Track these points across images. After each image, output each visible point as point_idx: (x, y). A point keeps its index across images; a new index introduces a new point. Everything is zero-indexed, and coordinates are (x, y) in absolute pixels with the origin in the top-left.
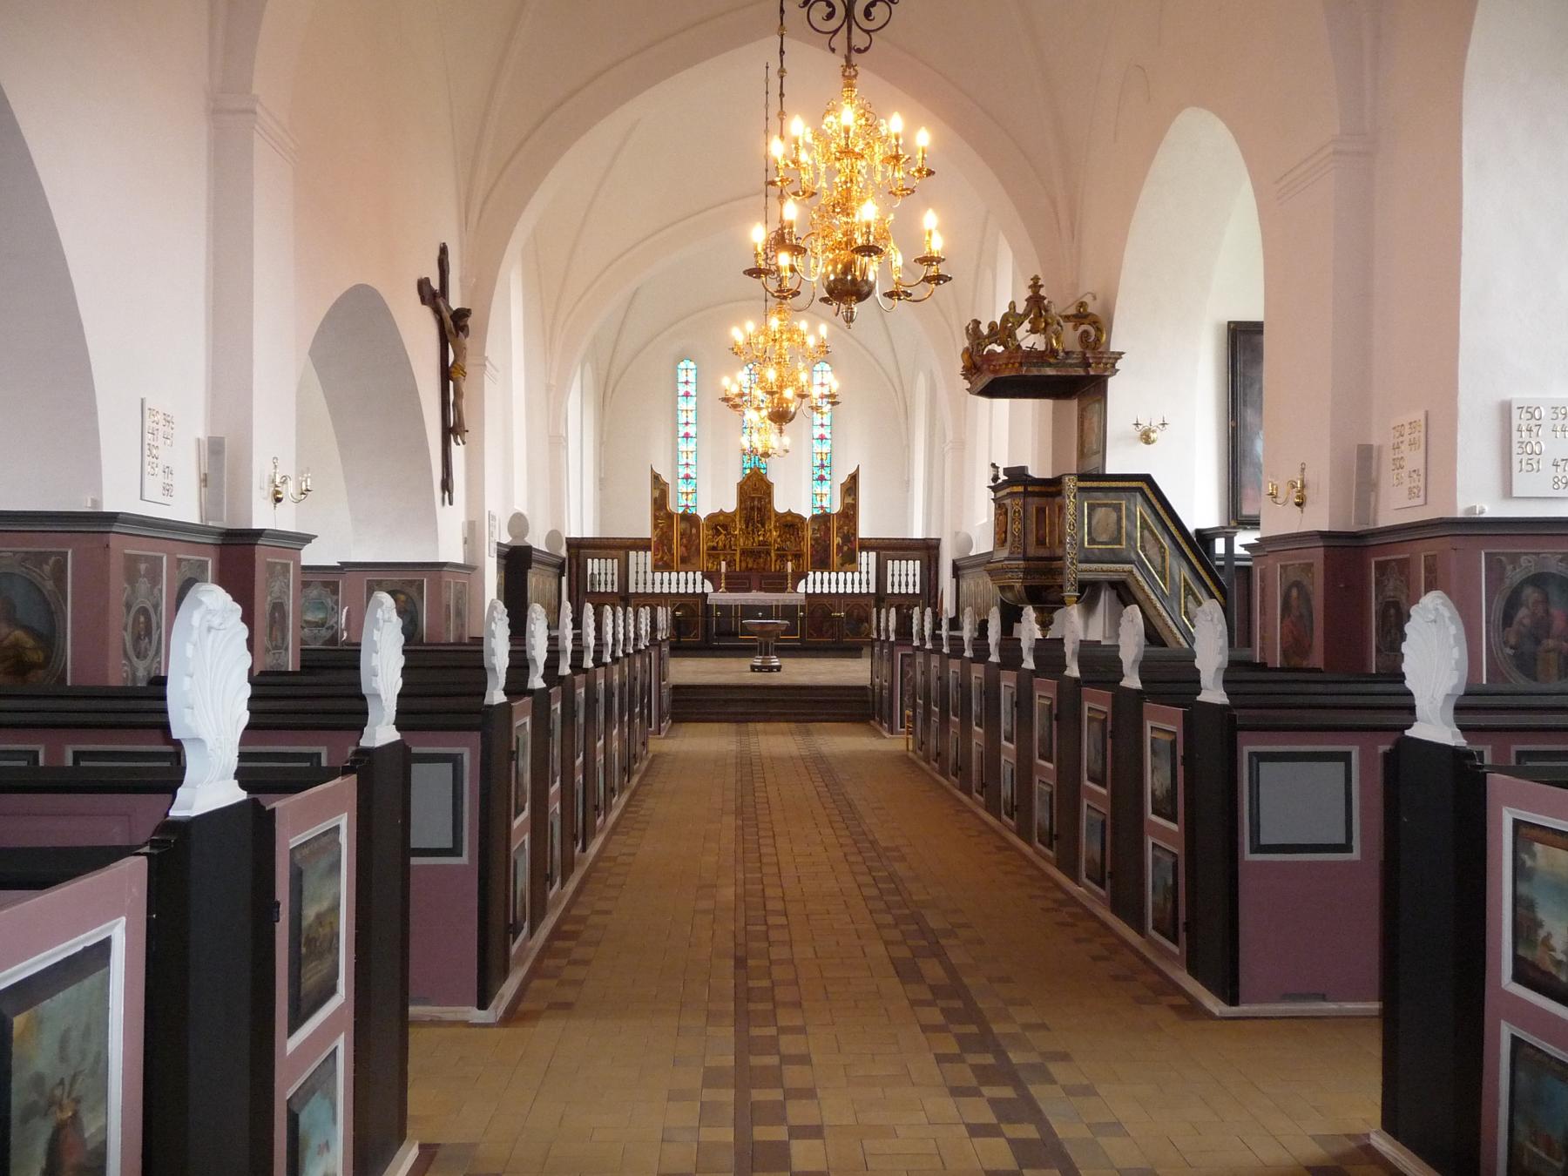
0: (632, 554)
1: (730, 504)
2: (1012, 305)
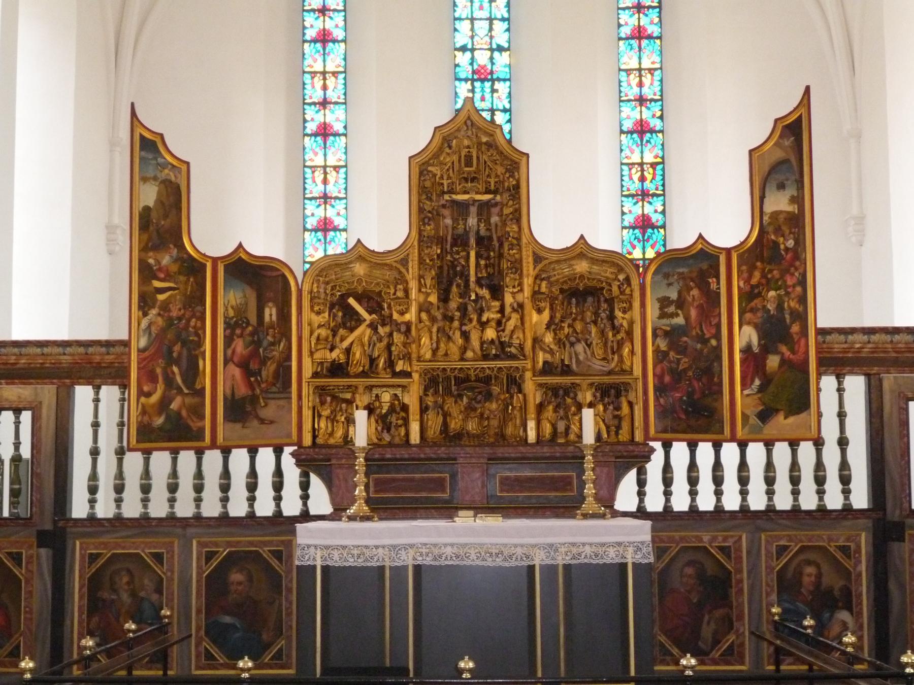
0: (83, 394)
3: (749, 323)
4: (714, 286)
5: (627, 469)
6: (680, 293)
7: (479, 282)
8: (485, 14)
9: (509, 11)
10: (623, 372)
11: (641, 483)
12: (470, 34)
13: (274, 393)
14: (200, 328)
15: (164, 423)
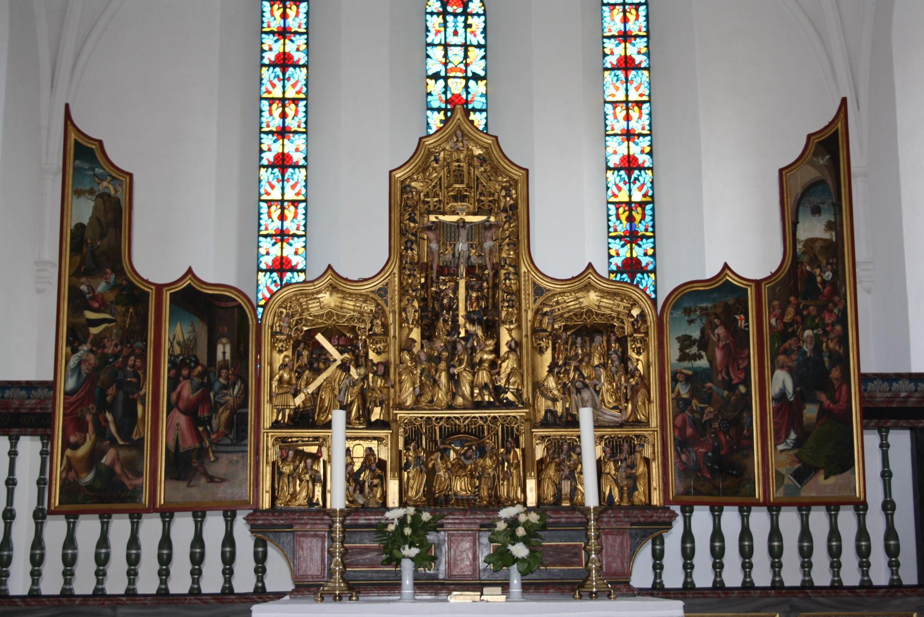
3: (782, 368)
4: (741, 324)
5: (644, 537)
6: (703, 331)
7: (469, 318)
8: (460, 40)
9: (485, 38)
10: (637, 423)
11: (658, 556)
12: (444, 60)
13: (227, 445)
14: (140, 368)
15: (94, 479)
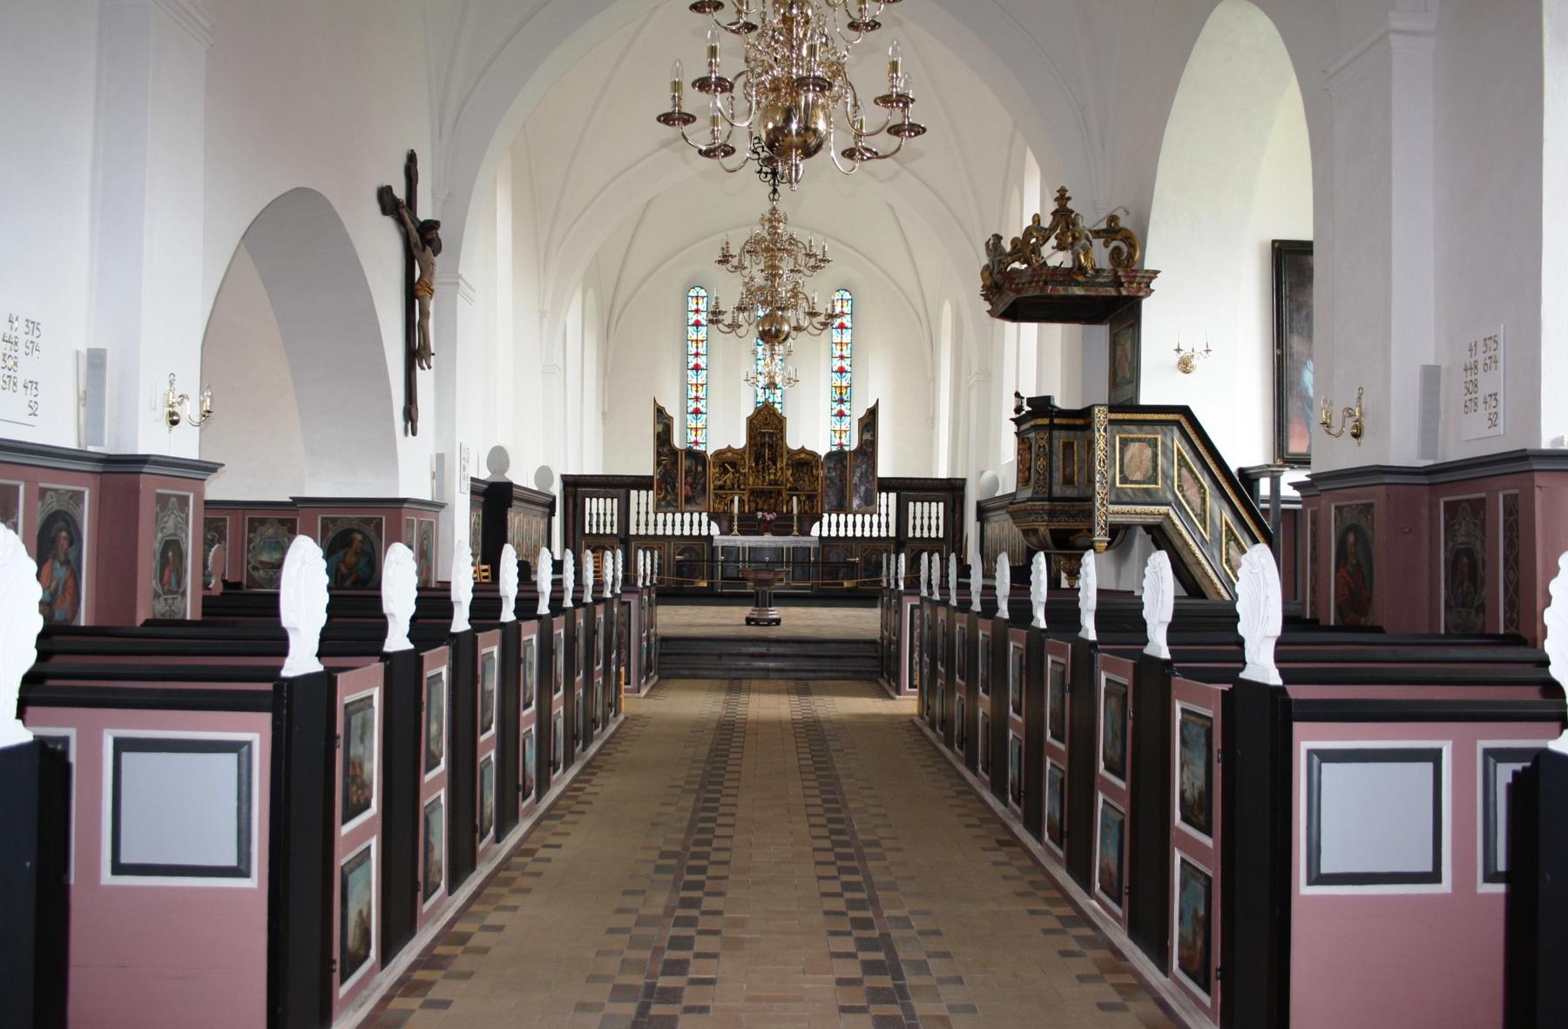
0: (633, 493)
1: (740, 441)
2: (1036, 219)
